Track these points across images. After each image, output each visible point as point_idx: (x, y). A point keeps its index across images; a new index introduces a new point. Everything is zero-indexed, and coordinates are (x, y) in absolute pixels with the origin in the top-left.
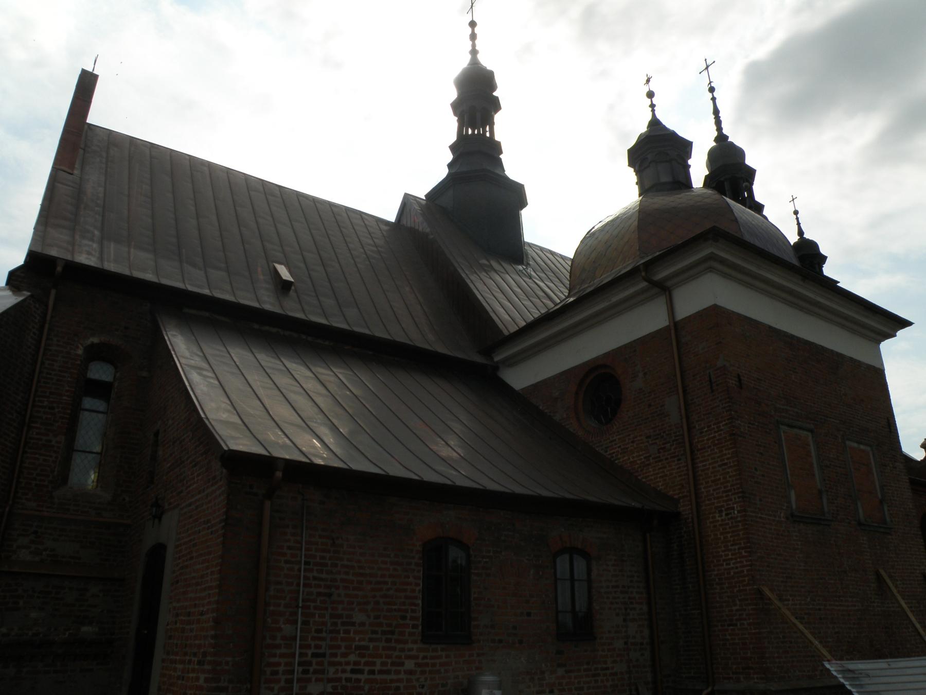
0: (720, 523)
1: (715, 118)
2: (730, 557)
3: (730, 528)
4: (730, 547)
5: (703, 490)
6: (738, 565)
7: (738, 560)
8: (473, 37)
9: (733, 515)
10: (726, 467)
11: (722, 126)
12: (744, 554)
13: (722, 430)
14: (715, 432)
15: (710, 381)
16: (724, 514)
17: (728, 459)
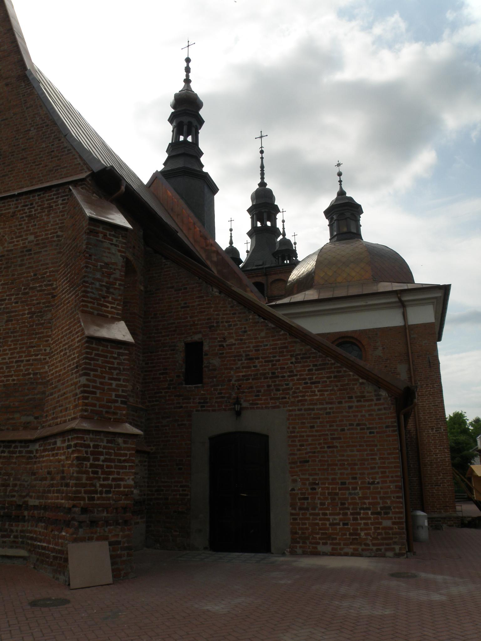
0: (432, 434)
1: (261, 171)
2: (438, 452)
3: (438, 438)
4: (438, 447)
5: (422, 417)
6: (443, 456)
7: (443, 454)
8: (188, 70)
9: (440, 431)
10: (437, 407)
11: (264, 177)
12: (446, 451)
13: (435, 388)
14: (431, 388)
15: (429, 362)
16: (434, 430)
17: (438, 403)
